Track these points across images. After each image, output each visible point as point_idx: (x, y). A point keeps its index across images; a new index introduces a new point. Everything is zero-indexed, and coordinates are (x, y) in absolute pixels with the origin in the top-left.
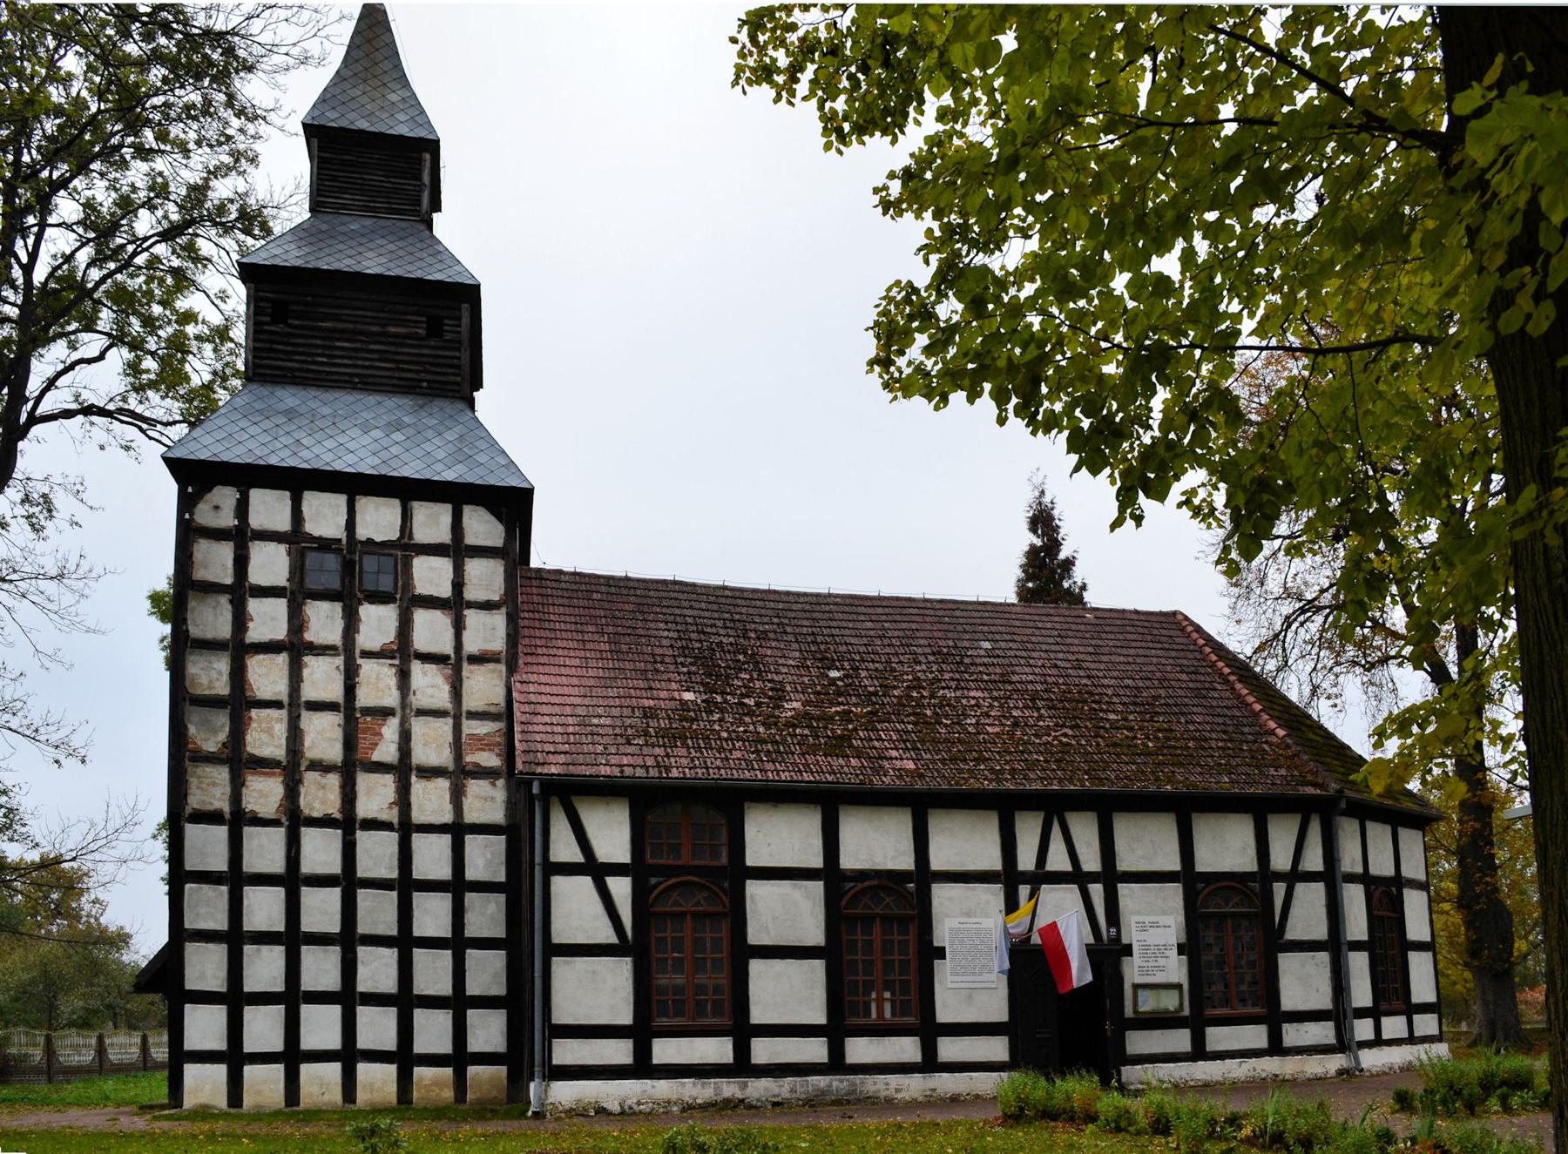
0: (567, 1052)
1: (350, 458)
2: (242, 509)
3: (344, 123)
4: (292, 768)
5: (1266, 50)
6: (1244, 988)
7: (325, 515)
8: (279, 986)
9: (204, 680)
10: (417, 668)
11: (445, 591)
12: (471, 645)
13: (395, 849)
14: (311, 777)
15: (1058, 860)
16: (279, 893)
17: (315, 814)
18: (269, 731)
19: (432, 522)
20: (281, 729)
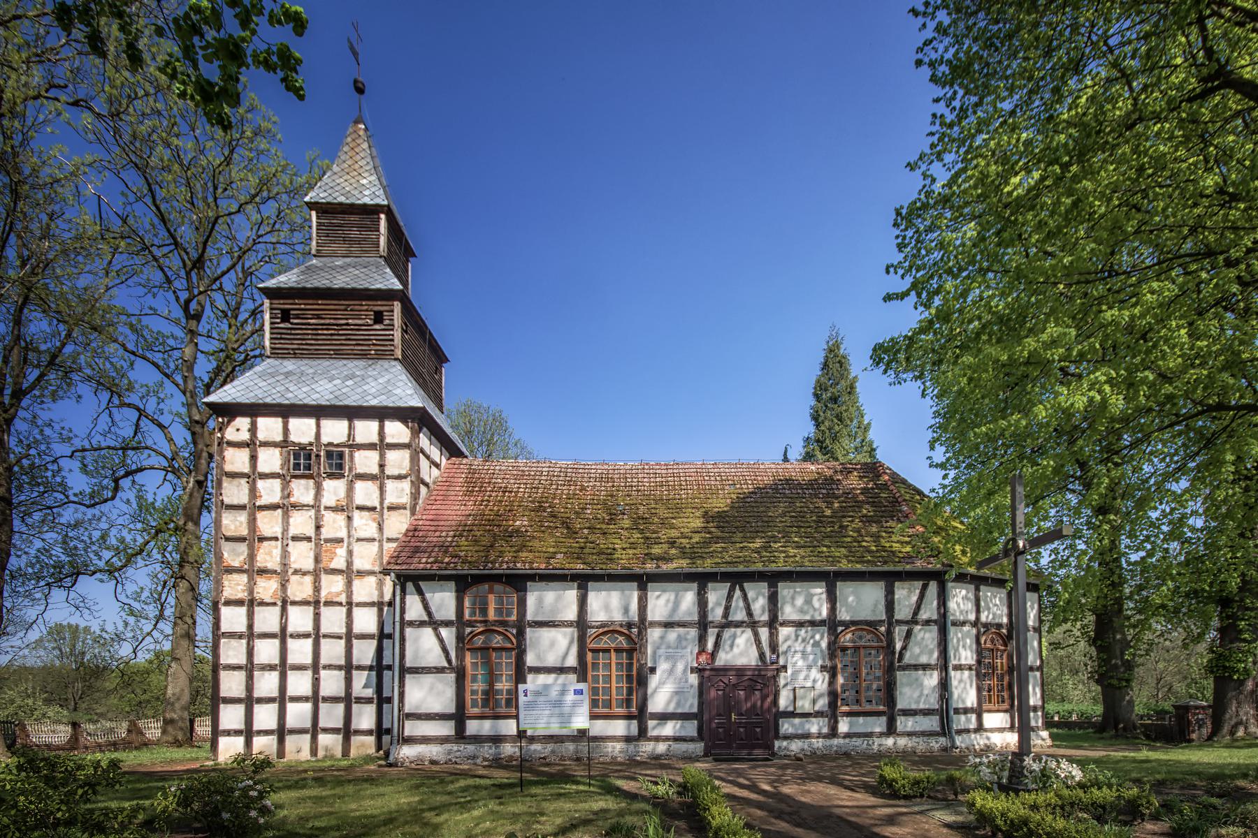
0: (411, 728)
1: (315, 396)
2: (253, 429)
3: (330, 199)
4: (283, 574)
5: (1027, 255)
6: (871, 693)
7: (302, 430)
8: (275, 693)
9: (232, 527)
10: (357, 515)
11: (375, 470)
12: (390, 499)
13: (344, 616)
14: (294, 579)
15: (739, 615)
16: (276, 643)
17: (297, 599)
18: (270, 554)
19: (367, 430)
20: (277, 552)
